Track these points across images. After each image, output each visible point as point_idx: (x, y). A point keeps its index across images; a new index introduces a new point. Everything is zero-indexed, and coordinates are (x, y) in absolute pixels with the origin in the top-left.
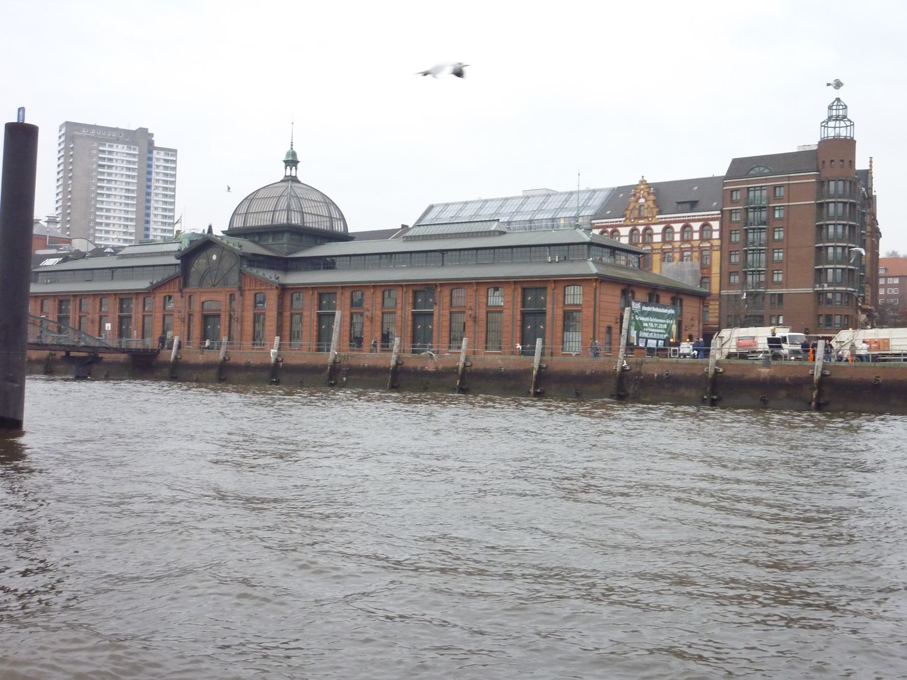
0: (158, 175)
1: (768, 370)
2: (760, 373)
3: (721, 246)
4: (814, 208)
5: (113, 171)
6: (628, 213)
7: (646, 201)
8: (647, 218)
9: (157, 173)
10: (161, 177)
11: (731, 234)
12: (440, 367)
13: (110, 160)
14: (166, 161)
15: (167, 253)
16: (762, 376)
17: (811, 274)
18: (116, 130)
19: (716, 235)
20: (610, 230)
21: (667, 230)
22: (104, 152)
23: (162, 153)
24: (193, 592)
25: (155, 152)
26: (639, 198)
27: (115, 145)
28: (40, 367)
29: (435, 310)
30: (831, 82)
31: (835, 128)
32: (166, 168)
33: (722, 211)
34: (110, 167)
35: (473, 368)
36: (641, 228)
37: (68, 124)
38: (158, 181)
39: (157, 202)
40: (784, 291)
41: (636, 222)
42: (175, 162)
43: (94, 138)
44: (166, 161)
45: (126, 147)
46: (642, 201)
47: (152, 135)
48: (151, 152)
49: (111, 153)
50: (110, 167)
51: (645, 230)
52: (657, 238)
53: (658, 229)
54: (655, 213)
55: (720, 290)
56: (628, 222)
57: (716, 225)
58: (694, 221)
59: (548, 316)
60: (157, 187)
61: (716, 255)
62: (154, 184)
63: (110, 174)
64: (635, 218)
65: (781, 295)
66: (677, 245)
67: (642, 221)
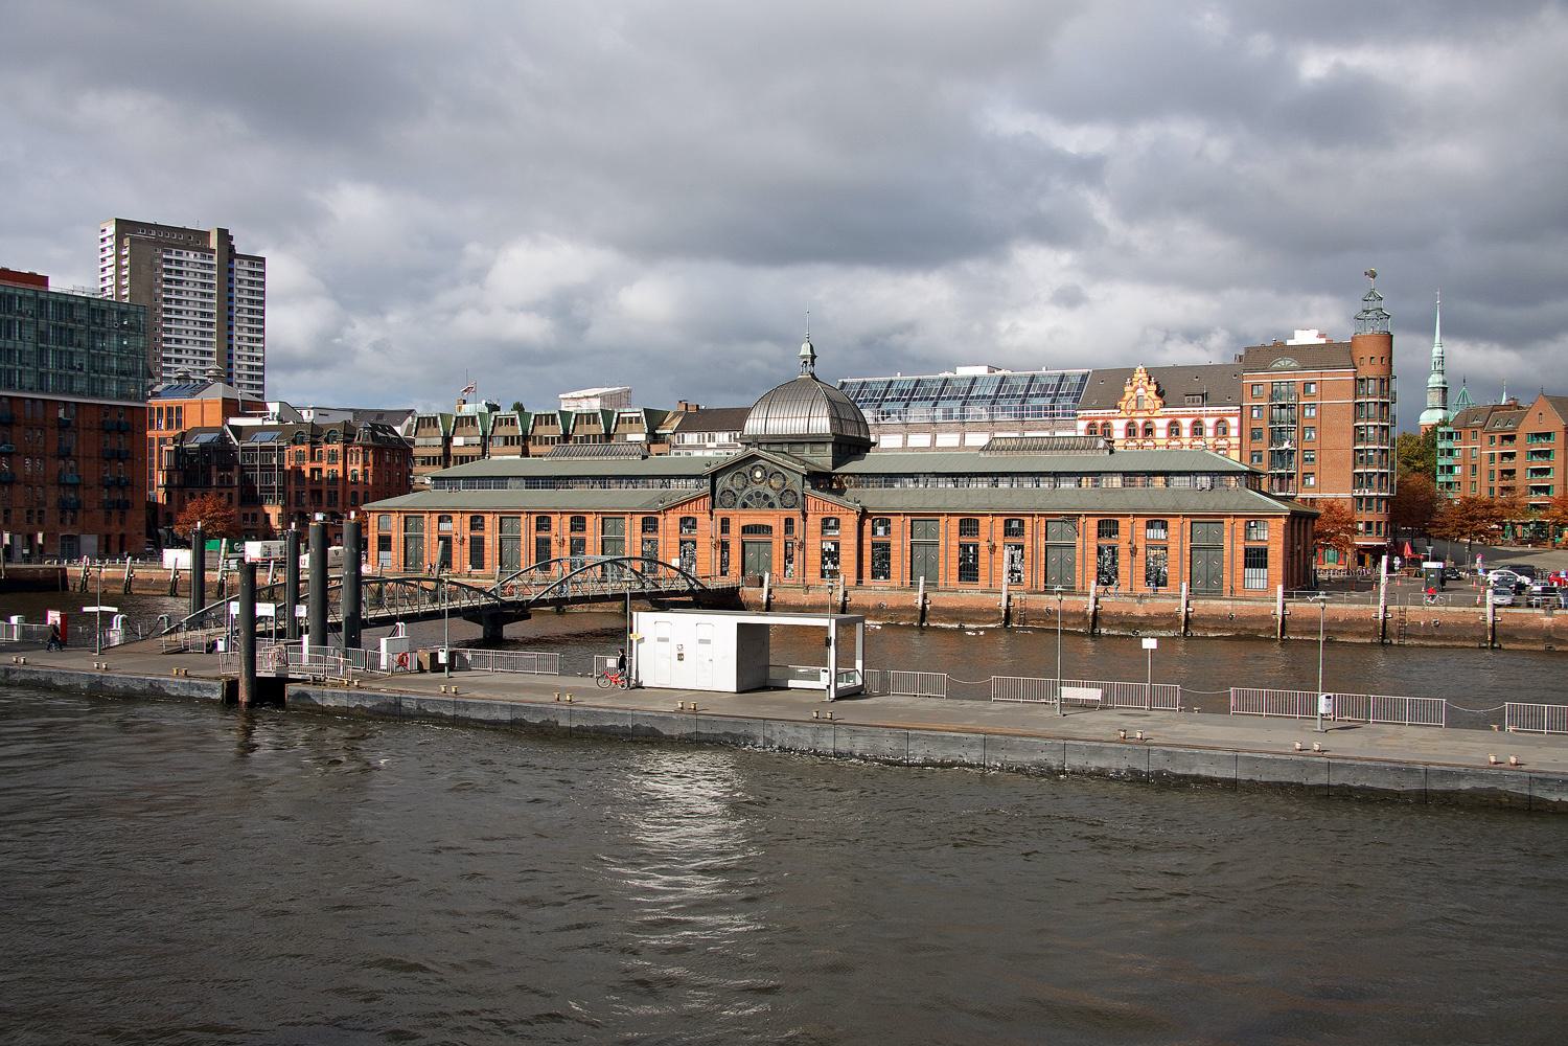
0: (241, 293)
1: (1551, 619)
2: (1541, 621)
3: (1241, 444)
4: (1352, 407)
5: (183, 287)
6: (1123, 404)
7: (1146, 391)
8: (1148, 410)
9: (240, 290)
10: (245, 295)
12: (1152, 613)
13: (179, 272)
14: (252, 273)
16: (1545, 625)
18: (183, 230)
19: (1234, 432)
20: (1100, 422)
22: (169, 261)
23: (246, 262)
24: (582, 937)
25: (236, 261)
26: (1137, 388)
27: (185, 252)
28: (646, 604)
29: (1079, 541)
32: (251, 283)
33: (1241, 407)
34: (179, 282)
35: (1195, 614)
36: (1140, 422)
38: (241, 300)
39: (240, 332)
40: (1317, 495)
41: (1134, 414)
42: (263, 274)
43: (157, 243)
44: (252, 273)
45: (199, 254)
46: (1141, 391)
47: (231, 238)
48: (231, 261)
49: (179, 263)
50: (179, 282)
56: (1123, 414)
57: (1234, 422)
58: (1183, 416)
59: (1226, 552)
60: (240, 310)
62: (237, 305)
63: (179, 292)
67: (1139, 414)
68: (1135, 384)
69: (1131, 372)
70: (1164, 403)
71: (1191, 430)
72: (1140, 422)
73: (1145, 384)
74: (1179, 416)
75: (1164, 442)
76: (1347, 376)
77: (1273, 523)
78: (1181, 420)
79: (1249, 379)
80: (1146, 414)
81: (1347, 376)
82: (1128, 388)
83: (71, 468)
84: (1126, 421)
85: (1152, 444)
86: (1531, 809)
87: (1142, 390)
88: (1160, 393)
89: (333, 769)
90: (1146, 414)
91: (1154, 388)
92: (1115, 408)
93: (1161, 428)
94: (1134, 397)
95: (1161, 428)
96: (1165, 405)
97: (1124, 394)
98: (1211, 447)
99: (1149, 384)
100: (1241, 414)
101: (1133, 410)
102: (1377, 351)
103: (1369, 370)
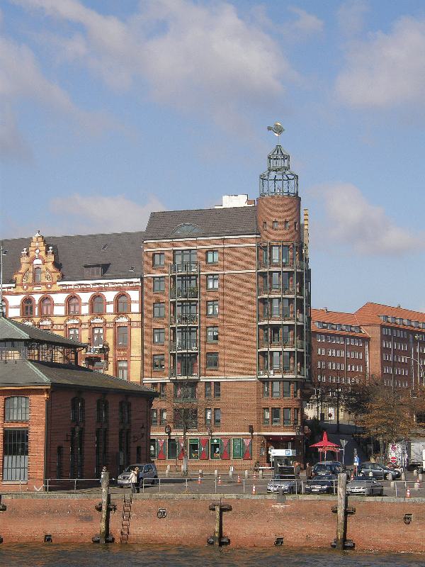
6: (19, 277)
7: (44, 263)
8: (45, 284)
11: (207, 305)
15: (123, 376)
17: (253, 358)
19: (135, 308)
21: (72, 300)
30: (272, 126)
31: (275, 180)
33: (142, 279)
36: (37, 298)
37: (27, 453)
51: (42, 300)
52: (59, 310)
53: (60, 298)
54: (56, 279)
55: (142, 377)
56: (20, 290)
57: (135, 295)
58: (83, 291)
61: (136, 334)
64: (29, 285)
65: (218, 384)
66: (85, 319)
68: (32, 254)
69: (28, 242)
70: (63, 276)
71: (23, 308)
72: (37, 298)
73: (43, 254)
74: (101, 289)
75: (61, 320)
76: (251, 242)
77: (34, 399)
78: (130, 292)
79: (151, 247)
80: (43, 288)
81: (251, 242)
82: (24, 260)
83: (36, 271)
84: (22, 297)
85: (76, 322)
86: (409, 558)
87: (40, 259)
88: (57, 265)
89: (212, 512)
90: (43, 288)
91: (52, 258)
92: (11, 282)
93: (58, 305)
94: (31, 269)
95: (58, 305)
96: (63, 278)
97: (20, 266)
98: (87, 326)
99: (46, 253)
100: (142, 287)
101: (29, 285)
102: (280, 215)
103: (278, 235)
